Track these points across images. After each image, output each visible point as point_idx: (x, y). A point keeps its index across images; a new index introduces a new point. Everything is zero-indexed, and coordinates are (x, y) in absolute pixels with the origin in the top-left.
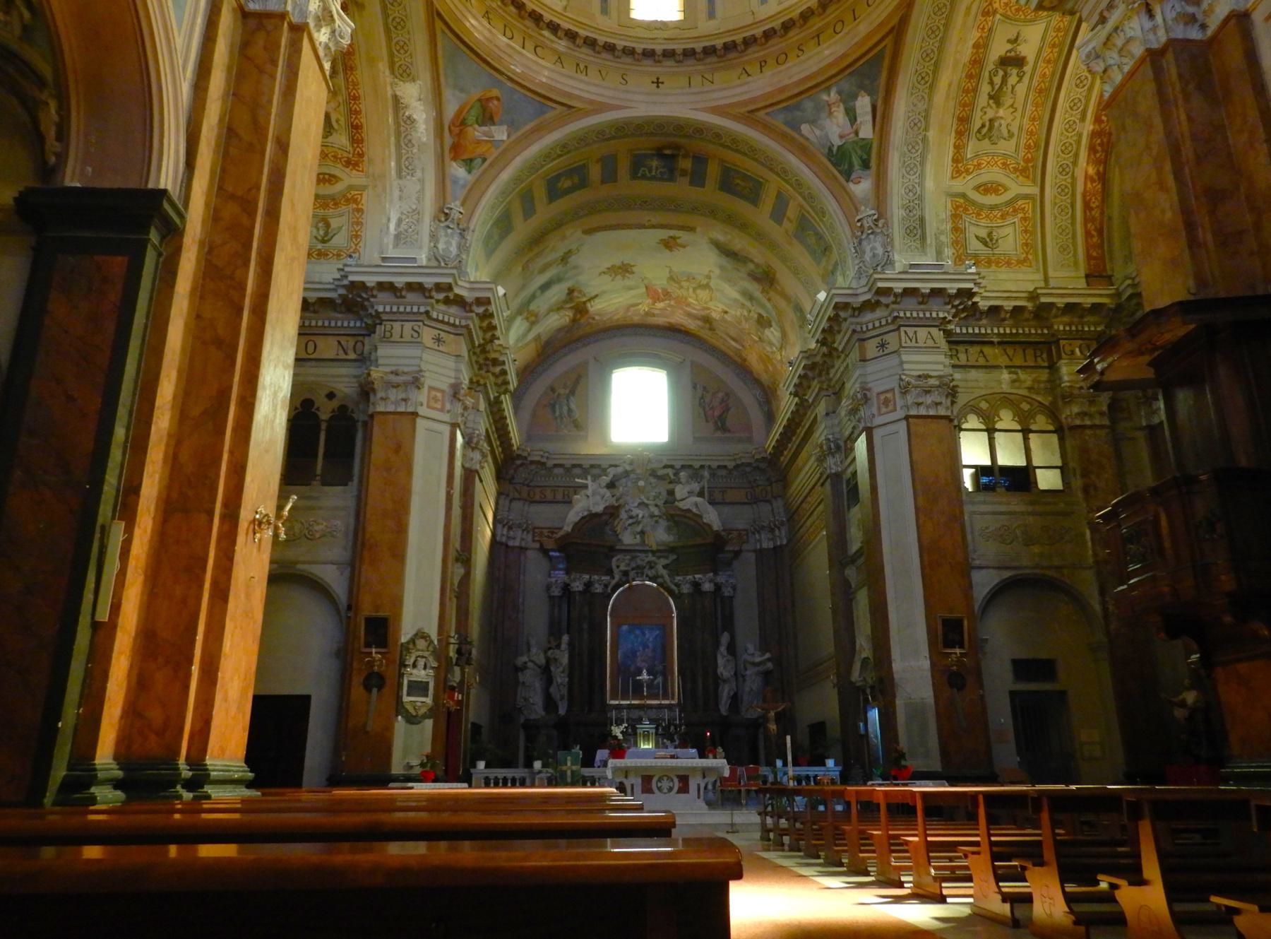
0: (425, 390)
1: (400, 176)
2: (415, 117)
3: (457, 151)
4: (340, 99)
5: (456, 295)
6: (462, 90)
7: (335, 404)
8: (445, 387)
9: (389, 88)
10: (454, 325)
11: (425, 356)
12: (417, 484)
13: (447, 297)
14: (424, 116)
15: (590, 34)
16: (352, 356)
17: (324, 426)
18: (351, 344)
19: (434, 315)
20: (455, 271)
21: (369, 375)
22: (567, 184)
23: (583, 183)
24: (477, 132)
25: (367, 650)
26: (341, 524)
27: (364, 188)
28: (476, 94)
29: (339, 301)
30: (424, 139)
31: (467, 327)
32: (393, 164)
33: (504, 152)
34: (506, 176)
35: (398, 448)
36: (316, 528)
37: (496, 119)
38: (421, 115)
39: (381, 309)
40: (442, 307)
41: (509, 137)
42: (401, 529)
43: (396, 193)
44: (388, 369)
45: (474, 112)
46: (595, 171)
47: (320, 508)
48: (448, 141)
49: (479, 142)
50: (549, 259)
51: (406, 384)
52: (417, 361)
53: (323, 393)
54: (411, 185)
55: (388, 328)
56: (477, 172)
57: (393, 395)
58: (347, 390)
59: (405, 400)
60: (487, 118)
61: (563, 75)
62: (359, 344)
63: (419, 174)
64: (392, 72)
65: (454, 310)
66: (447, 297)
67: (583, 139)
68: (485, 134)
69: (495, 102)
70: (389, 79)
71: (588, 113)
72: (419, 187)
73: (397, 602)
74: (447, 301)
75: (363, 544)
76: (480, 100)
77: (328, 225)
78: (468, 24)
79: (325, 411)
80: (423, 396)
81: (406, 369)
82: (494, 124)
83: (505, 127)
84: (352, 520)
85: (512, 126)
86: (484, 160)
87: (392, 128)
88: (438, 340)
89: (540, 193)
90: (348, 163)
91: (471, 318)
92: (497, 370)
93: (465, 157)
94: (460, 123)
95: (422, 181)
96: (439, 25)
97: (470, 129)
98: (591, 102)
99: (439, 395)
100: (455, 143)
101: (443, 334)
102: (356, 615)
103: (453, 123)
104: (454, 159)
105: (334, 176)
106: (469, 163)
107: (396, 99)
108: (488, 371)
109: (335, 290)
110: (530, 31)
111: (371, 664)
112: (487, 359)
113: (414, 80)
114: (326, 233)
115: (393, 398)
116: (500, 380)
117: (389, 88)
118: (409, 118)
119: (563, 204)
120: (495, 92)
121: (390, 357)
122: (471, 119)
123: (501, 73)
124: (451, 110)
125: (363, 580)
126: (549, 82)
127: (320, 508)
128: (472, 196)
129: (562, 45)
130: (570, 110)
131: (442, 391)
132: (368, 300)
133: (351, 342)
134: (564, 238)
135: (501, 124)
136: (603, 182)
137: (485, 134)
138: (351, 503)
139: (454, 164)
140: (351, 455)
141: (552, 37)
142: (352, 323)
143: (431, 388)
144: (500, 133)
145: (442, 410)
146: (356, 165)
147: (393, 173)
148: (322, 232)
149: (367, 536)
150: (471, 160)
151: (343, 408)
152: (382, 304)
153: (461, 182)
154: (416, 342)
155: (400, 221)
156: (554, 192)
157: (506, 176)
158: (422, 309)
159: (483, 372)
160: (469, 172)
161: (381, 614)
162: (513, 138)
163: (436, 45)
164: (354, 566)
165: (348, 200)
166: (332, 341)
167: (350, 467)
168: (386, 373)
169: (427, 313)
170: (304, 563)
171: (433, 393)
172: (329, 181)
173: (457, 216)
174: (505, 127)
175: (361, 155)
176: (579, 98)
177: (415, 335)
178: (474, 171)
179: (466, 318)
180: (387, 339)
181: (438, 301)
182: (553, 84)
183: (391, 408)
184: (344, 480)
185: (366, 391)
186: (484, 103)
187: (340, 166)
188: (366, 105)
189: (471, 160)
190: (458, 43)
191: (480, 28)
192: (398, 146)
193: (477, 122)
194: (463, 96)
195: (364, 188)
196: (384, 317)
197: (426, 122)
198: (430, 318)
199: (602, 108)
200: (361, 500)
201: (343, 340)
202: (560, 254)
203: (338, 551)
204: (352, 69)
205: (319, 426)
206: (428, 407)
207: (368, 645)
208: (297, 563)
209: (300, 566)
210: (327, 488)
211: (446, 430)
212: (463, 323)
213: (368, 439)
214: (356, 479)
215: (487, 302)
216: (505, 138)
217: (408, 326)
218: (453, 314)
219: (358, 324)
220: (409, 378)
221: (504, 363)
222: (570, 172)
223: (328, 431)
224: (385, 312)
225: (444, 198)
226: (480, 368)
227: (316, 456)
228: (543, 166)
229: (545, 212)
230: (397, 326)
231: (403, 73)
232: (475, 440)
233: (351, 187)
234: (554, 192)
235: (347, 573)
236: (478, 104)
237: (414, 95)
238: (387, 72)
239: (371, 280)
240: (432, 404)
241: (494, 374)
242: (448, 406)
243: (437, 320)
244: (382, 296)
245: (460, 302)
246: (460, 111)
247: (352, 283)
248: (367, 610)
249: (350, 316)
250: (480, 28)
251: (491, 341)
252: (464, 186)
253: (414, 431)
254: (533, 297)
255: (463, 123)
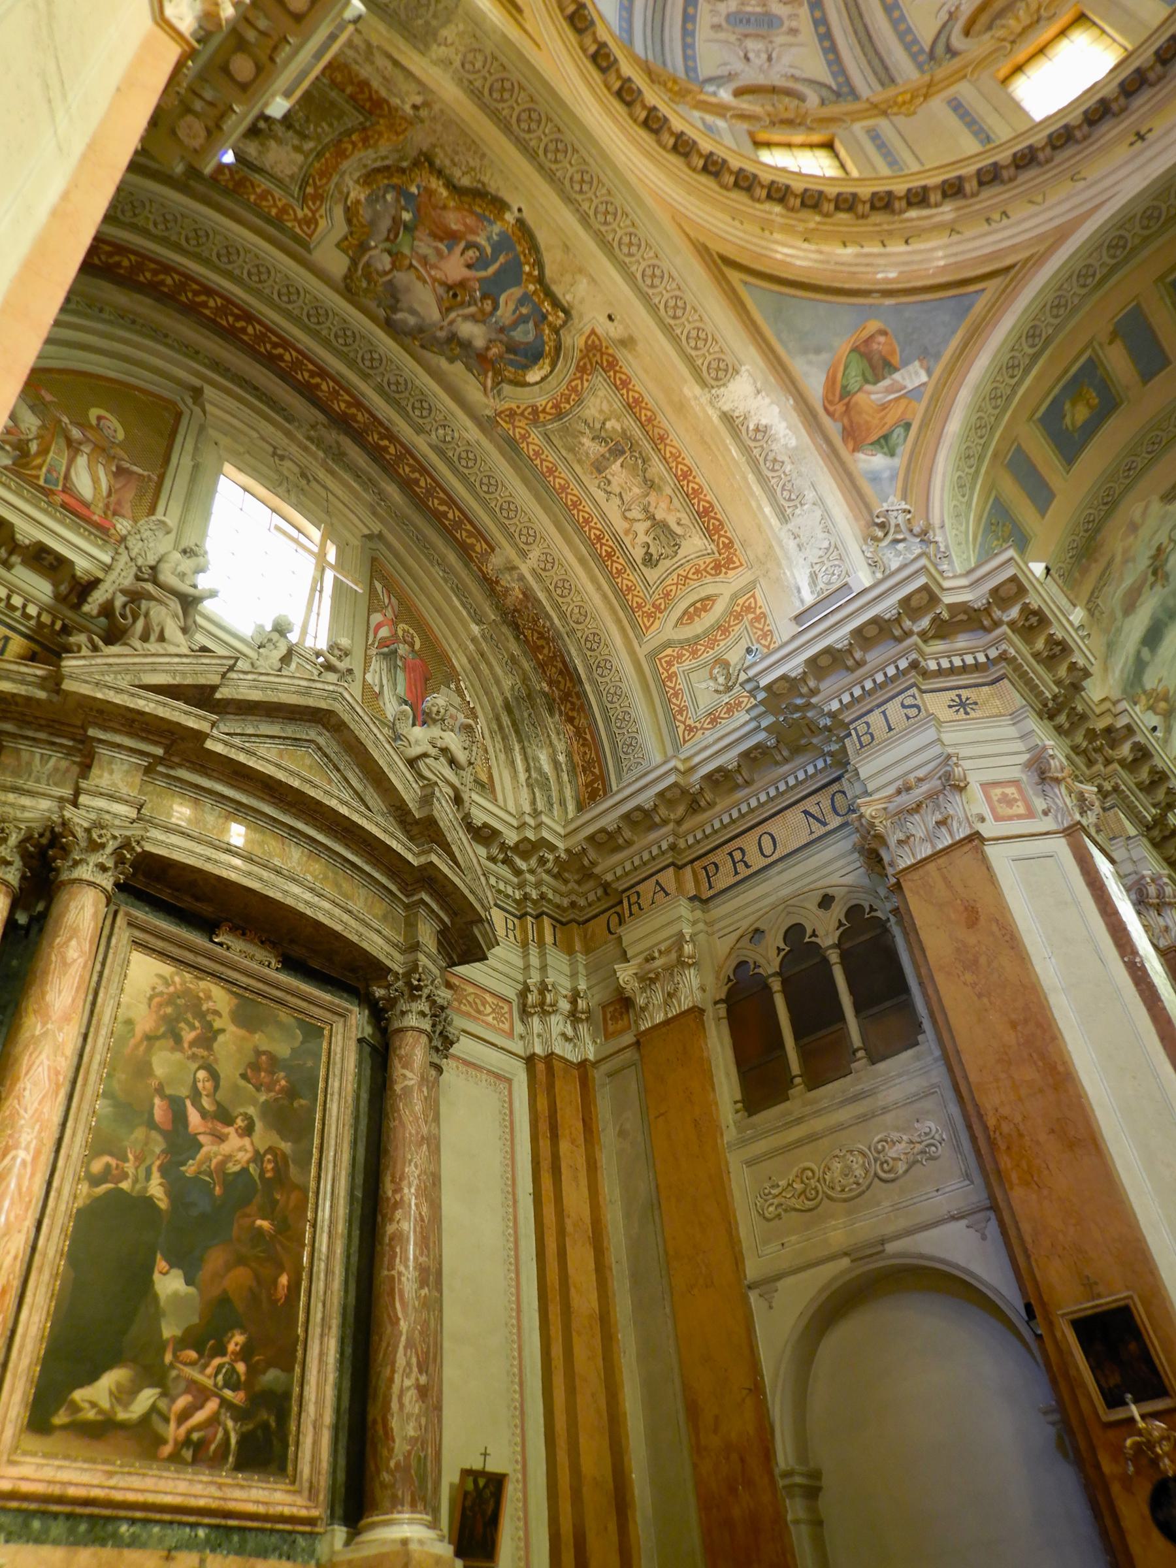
0: (975, 789)
1: (784, 518)
2: (764, 422)
3: (855, 436)
4: (668, 491)
5: (950, 607)
6: (818, 351)
7: (838, 911)
8: (1016, 773)
9: (710, 411)
10: (977, 667)
11: (946, 738)
12: (1048, 969)
13: (937, 619)
14: (776, 409)
15: (979, 165)
16: (835, 822)
17: (834, 957)
18: (826, 804)
19: (932, 665)
20: (924, 561)
21: (861, 816)
22: (1079, 414)
23: (1109, 404)
24: (875, 394)
25: (1119, 1414)
26: (935, 1124)
27: (753, 584)
28: (843, 345)
29: (771, 742)
30: (793, 443)
31: (1003, 657)
32: (768, 510)
33: (935, 398)
34: (955, 426)
35: (972, 916)
36: (892, 1153)
37: (896, 360)
38: (772, 413)
39: (835, 706)
40: (938, 646)
41: (929, 373)
42: (1059, 1077)
43: (792, 545)
44: (891, 790)
45: (854, 371)
46: (1118, 362)
47: (885, 1110)
48: (833, 429)
49: (884, 407)
50: (1128, 582)
51: (933, 796)
52: (936, 750)
53: (812, 905)
54: (807, 519)
55: (862, 729)
56: (904, 450)
57: (919, 826)
58: (849, 880)
59: (941, 823)
60: (878, 366)
61: (968, 240)
62: (838, 797)
63: (810, 495)
64: (704, 384)
65: (962, 641)
66: (937, 619)
67: (1058, 306)
68: (888, 391)
69: (882, 339)
70: (704, 398)
71: (1035, 261)
72: (818, 513)
73: (1136, 1256)
74: (942, 629)
75: (992, 1144)
76: (855, 349)
77: (726, 665)
78: (779, 256)
79: (826, 930)
80: (975, 803)
81: (921, 773)
82: (896, 370)
83: (917, 363)
84: (954, 1110)
85: (927, 355)
86: (908, 426)
87: (742, 460)
88: (962, 705)
89: (1041, 452)
90: (718, 567)
91: (1004, 638)
92: (1125, 750)
93: (874, 438)
94: (840, 397)
95: (820, 502)
96: (734, 276)
97: (860, 398)
98: (1040, 238)
99: (1011, 791)
100: (843, 425)
101: (965, 693)
102: (1051, 1325)
103: (828, 401)
104: (855, 449)
105: (708, 598)
106: (885, 443)
107: (727, 418)
108: (1108, 762)
109: (757, 729)
110: (886, 227)
111: (1145, 1454)
112: (1091, 735)
113: (736, 372)
114: (728, 677)
115: (920, 833)
116: (1144, 775)
117: (710, 411)
118: (757, 430)
119: (1097, 458)
120: (873, 326)
121: (884, 766)
122: (854, 382)
123: (866, 293)
124: (815, 384)
125: (1026, 1227)
126: (952, 260)
127: (885, 1110)
128: (914, 482)
129: (947, 211)
130: (1007, 274)
131: (1015, 783)
132: (808, 706)
133: (824, 799)
134: (1134, 528)
135: (906, 363)
136: (1147, 376)
137: (888, 391)
138: (938, 1075)
139: (861, 456)
140: (906, 989)
141: (925, 212)
142: (804, 770)
143: (985, 786)
144: (914, 376)
145: (1030, 814)
146: (730, 560)
147: (774, 521)
148: (721, 680)
149: (991, 1122)
150: (886, 437)
151: (854, 912)
152: (833, 695)
153: (886, 474)
154: (917, 715)
155: (813, 577)
156: (1070, 447)
157: (955, 426)
158: (903, 664)
159: (1099, 767)
160: (892, 454)
161: (1107, 1301)
162: (938, 370)
163: (743, 305)
164: (995, 1208)
165: (739, 617)
166: (795, 817)
167: (909, 1006)
168: (889, 799)
169: (914, 665)
170: (897, 1237)
171: (997, 792)
172: (705, 609)
173: (901, 519)
174: (917, 363)
175: (729, 545)
176: (1013, 248)
177: (914, 711)
178: (899, 450)
179: (995, 643)
180: (869, 743)
181: (923, 635)
182: (959, 258)
183: (925, 851)
184: (909, 1037)
185: (872, 855)
186: (863, 351)
187: (709, 579)
188: (705, 475)
189: (886, 437)
190: (776, 288)
191: (801, 254)
192: (763, 480)
193: (867, 381)
194: (825, 356)
195: (753, 584)
196: (847, 717)
197: (783, 416)
198: (925, 674)
199: (1062, 234)
200: (951, 1061)
201: (809, 805)
202: (1143, 563)
203: (949, 1187)
204: (662, 438)
205: (825, 961)
206: (998, 818)
207: (1114, 1400)
208: (883, 1242)
209: (891, 1248)
210: (882, 1066)
211: (1060, 846)
212: (993, 653)
213: (911, 931)
214: (927, 1025)
215: (1022, 590)
216: (924, 378)
217: (893, 708)
218: (966, 647)
219: (820, 764)
220: (935, 783)
221: (1129, 730)
222: (1074, 388)
223: (844, 957)
224: (844, 707)
225: (867, 506)
226: (1090, 763)
227: (842, 1018)
228: (1014, 389)
229: (1073, 487)
230: (875, 719)
231: (715, 374)
232: (1152, 890)
233: (735, 597)
234: (1070, 447)
235: (993, 1227)
236: (855, 356)
237: (751, 396)
238: (697, 390)
239: (794, 666)
240: (1003, 810)
241: (1122, 762)
242: (1040, 804)
243: (940, 672)
244: (828, 685)
245: (969, 619)
246: (831, 382)
247: (769, 688)
248: (1069, 1301)
249: (800, 760)
250: (801, 254)
251: (1076, 687)
252: (893, 477)
253: (989, 868)
254: (1140, 666)
255: (846, 393)
